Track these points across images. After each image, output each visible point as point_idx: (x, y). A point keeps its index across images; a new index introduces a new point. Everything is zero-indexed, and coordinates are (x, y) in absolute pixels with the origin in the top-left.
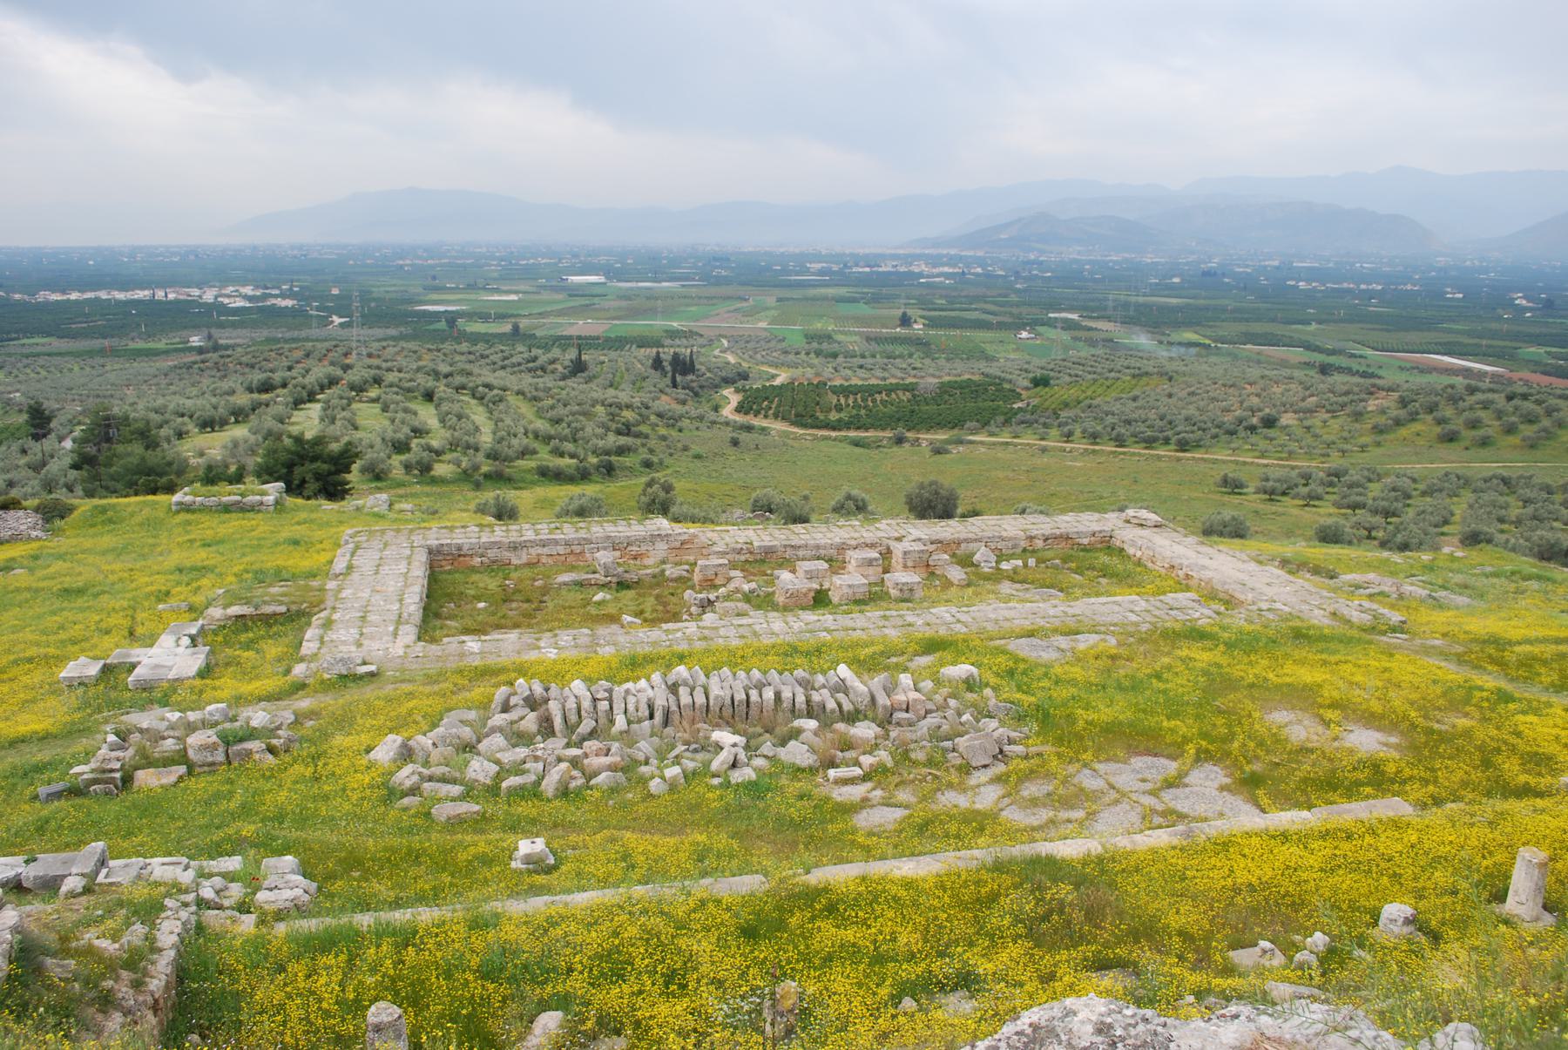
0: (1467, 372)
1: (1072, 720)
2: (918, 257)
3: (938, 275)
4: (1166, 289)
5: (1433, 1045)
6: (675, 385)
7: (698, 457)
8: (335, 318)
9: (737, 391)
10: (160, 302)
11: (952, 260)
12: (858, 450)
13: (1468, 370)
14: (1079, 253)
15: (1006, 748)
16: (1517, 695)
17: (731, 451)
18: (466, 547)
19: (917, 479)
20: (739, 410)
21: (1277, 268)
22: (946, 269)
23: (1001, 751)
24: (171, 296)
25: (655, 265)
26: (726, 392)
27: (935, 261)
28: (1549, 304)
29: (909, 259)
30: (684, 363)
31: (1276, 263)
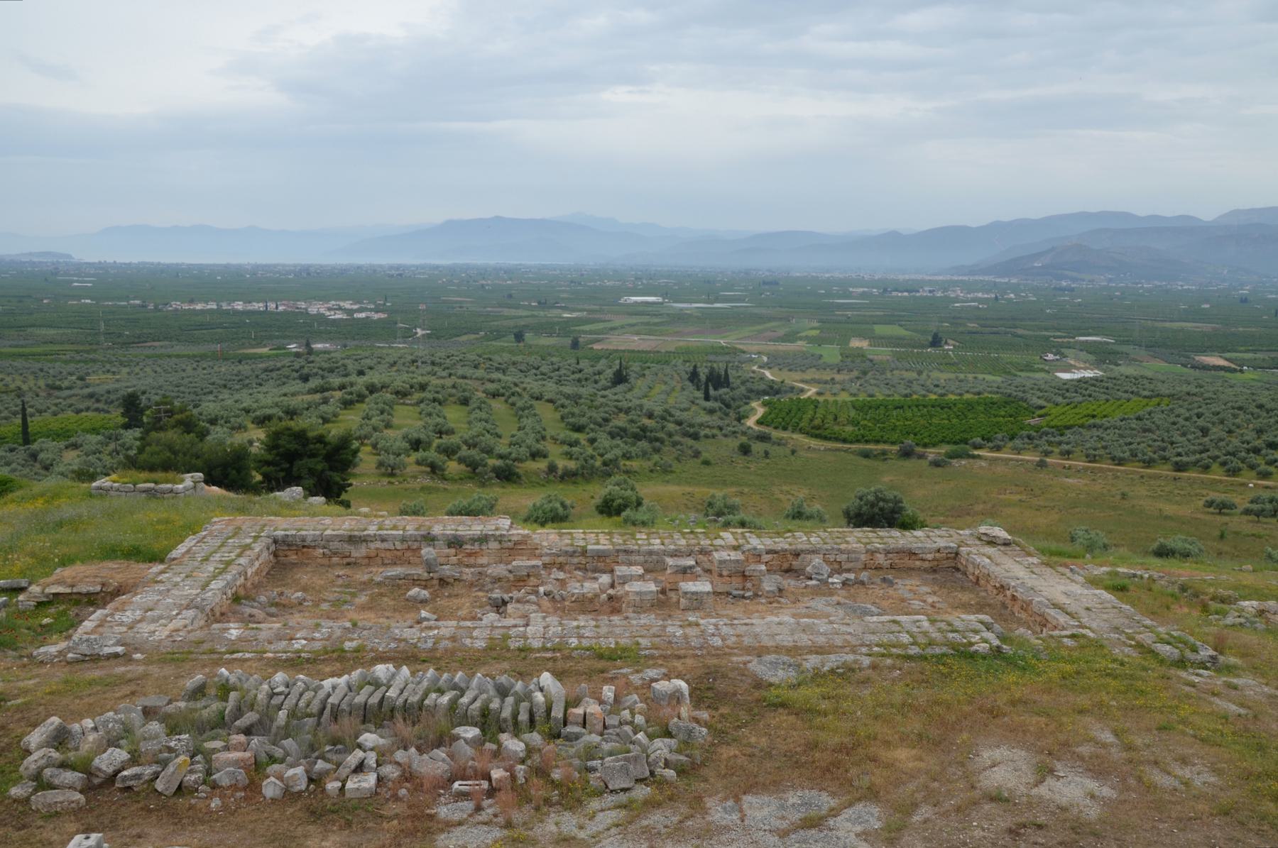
3: (973, 300)
6: (707, 398)
7: (706, 463)
8: (418, 330)
9: (765, 404)
10: (272, 313)
12: (865, 462)
14: (1110, 280)
15: (658, 771)
16: (802, 832)
17: (740, 460)
18: (309, 539)
20: (759, 422)
22: (980, 295)
23: (652, 773)
24: (281, 308)
25: (708, 286)
26: (754, 404)
27: (968, 287)
29: (945, 286)
30: (719, 376)
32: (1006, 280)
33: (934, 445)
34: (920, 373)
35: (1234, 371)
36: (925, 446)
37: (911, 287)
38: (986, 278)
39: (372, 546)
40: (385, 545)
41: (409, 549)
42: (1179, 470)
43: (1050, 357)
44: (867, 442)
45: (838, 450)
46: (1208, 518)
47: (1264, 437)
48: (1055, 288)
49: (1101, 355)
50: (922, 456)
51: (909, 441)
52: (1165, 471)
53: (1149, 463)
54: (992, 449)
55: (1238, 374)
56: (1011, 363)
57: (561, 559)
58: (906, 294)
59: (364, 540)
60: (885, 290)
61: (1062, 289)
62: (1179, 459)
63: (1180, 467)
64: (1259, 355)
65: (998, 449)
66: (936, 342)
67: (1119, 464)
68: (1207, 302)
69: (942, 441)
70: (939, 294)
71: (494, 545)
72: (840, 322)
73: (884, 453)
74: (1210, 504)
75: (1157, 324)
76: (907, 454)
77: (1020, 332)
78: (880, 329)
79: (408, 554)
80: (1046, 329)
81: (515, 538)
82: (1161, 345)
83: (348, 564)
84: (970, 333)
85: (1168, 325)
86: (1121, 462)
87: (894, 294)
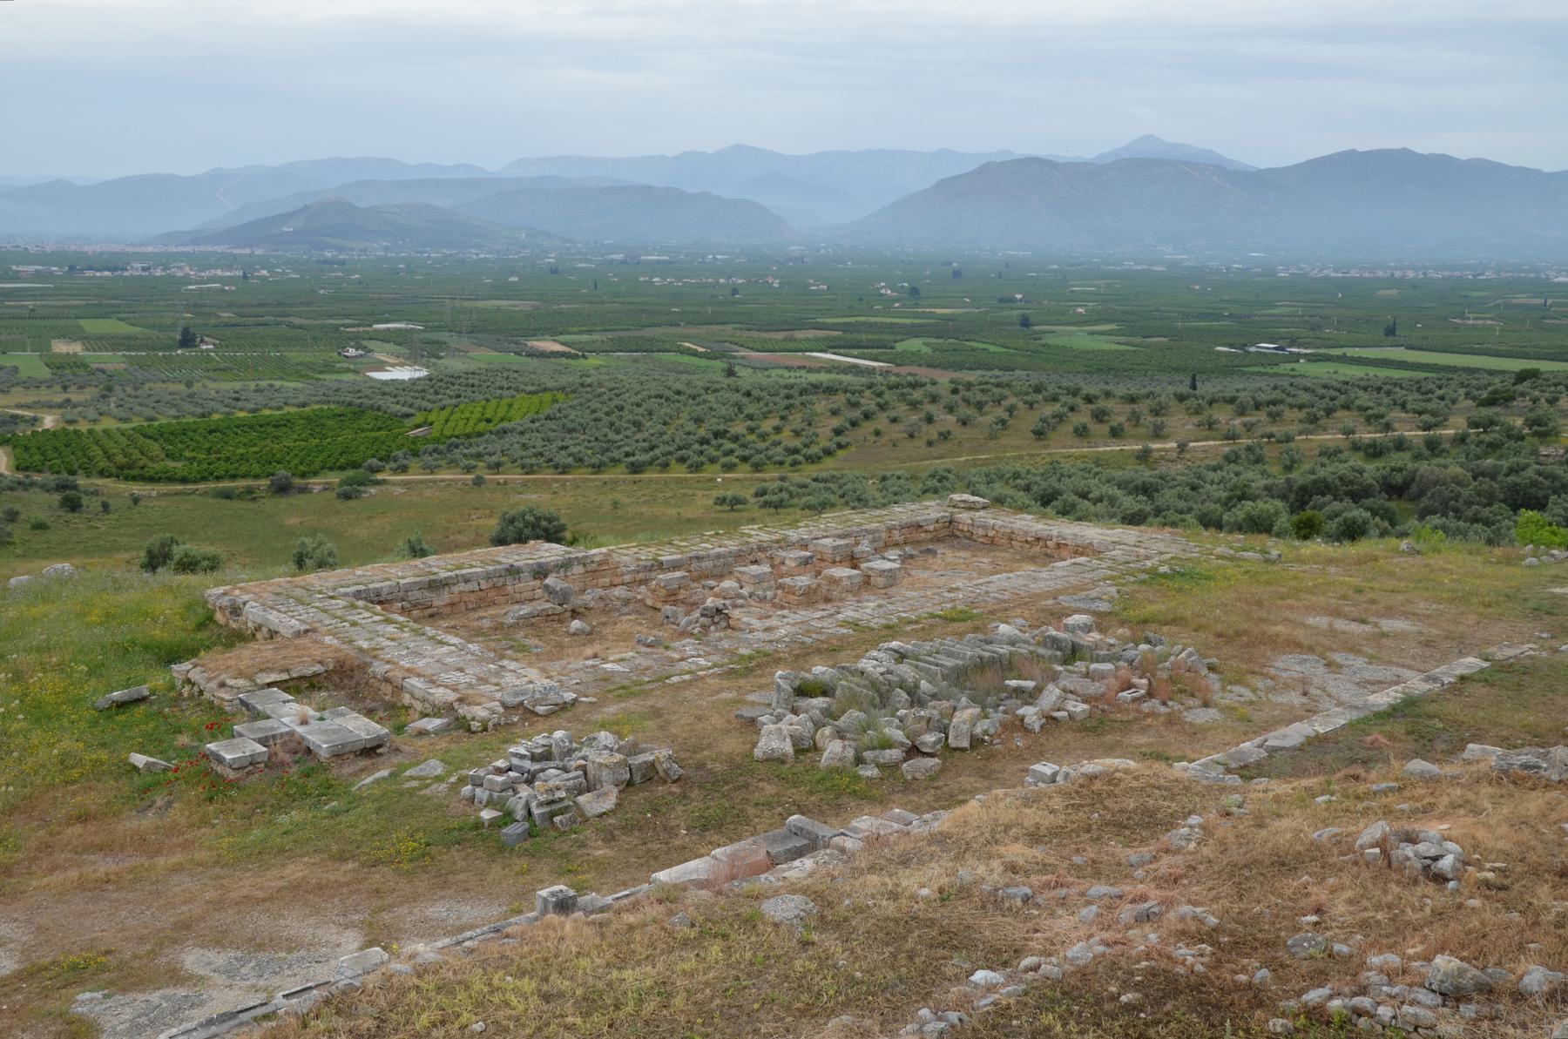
0: (854, 369)
1: (364, 986)
2: (179, 256)
4: (503, 290)
5: (11, 810)
11: (230, 262)
13: (855, 366)
14: (387, 249)
19: (1206, 533)
21: (624, 262)
22: (219, 272)
27: (200, 262)
28: (914, 291)
29: (165, 260)
31: (621, 256)
32: (248, 251)
33: (315, 474)
34: (189, 384)
35: (575, 357)
36: (304, 475)
37: (114, 263)
38: (219, 249)
39: (456, 589)
40: (469, 587)
41: (494, 587)
42: (635, 472)
43: (352, 352)
44: (218, 478)
45: (178, 493)
46: (724, 515)
47: (706, 425)
48: (319, 262)
49: (415, 349)
50: (304, 490)
51: (282, 472)
52: (618, 473)
53: (598, 468)
54: (394, 471)
55: (582, 361)
56: (302, 364)
57: (641, 576)
58: (107, 273)
59: (444, 584)
60: (72, 268)
61: (326, 262)
62: (632, 459)
63: (636, 468)
64: (595, 337)
65: (403, 469)
66: (187, 340)
67: (563, 473)
68: (513, 273)
69: (322, 468)
70: (158, 273)
71: (578, 569)
72: (21, 318)
73: (249, 491)
74: (721, 501)
75: (466, 304)
76: (282, 489)
77: (296, 321)
78: (90, 326)
79: (493, 593)
80: (331, 316)
81: (597, 559)
82: (486, 330)
83: (431, 616)
84: (227, 325)
85: (479, 304)
86: (565, 469)
87: (89, 273)
